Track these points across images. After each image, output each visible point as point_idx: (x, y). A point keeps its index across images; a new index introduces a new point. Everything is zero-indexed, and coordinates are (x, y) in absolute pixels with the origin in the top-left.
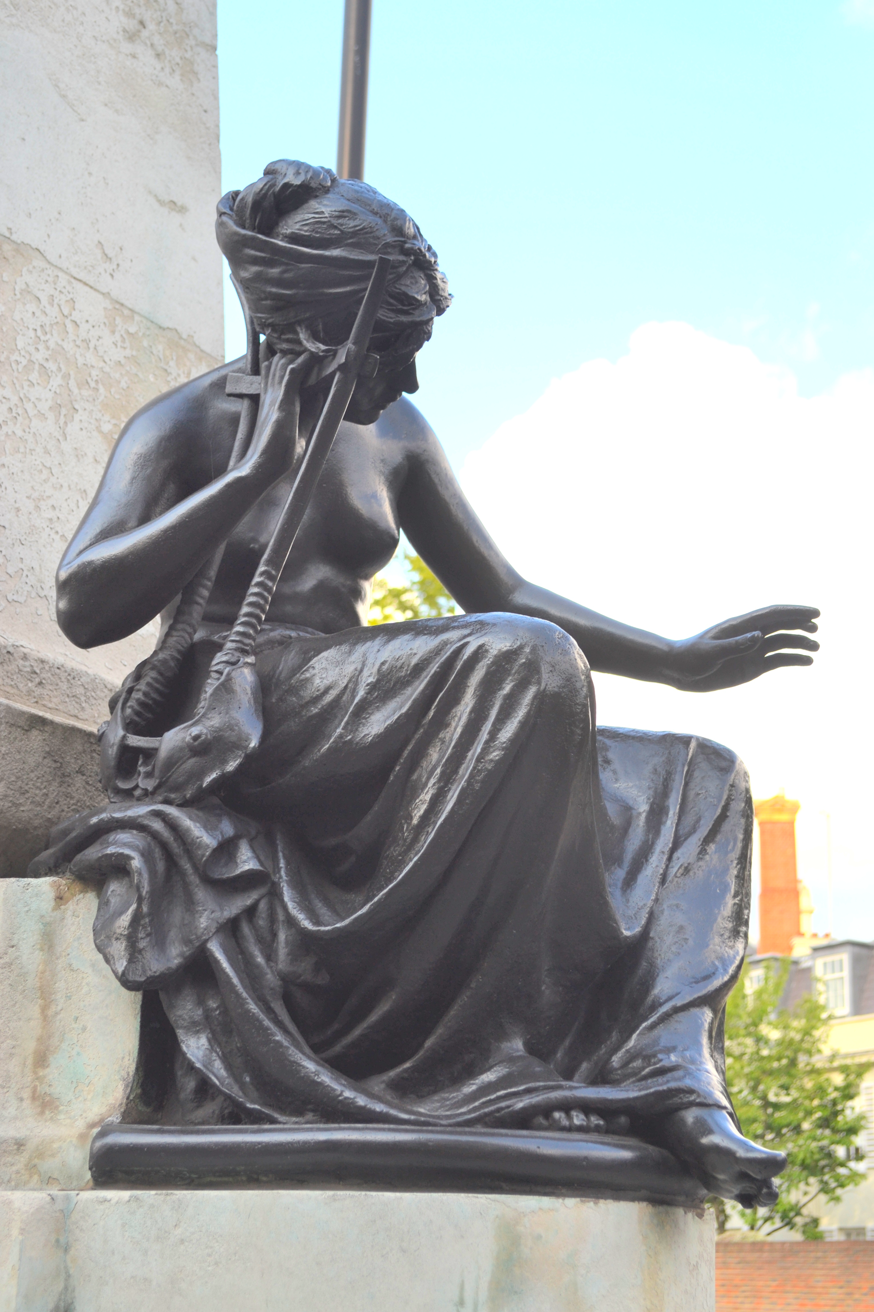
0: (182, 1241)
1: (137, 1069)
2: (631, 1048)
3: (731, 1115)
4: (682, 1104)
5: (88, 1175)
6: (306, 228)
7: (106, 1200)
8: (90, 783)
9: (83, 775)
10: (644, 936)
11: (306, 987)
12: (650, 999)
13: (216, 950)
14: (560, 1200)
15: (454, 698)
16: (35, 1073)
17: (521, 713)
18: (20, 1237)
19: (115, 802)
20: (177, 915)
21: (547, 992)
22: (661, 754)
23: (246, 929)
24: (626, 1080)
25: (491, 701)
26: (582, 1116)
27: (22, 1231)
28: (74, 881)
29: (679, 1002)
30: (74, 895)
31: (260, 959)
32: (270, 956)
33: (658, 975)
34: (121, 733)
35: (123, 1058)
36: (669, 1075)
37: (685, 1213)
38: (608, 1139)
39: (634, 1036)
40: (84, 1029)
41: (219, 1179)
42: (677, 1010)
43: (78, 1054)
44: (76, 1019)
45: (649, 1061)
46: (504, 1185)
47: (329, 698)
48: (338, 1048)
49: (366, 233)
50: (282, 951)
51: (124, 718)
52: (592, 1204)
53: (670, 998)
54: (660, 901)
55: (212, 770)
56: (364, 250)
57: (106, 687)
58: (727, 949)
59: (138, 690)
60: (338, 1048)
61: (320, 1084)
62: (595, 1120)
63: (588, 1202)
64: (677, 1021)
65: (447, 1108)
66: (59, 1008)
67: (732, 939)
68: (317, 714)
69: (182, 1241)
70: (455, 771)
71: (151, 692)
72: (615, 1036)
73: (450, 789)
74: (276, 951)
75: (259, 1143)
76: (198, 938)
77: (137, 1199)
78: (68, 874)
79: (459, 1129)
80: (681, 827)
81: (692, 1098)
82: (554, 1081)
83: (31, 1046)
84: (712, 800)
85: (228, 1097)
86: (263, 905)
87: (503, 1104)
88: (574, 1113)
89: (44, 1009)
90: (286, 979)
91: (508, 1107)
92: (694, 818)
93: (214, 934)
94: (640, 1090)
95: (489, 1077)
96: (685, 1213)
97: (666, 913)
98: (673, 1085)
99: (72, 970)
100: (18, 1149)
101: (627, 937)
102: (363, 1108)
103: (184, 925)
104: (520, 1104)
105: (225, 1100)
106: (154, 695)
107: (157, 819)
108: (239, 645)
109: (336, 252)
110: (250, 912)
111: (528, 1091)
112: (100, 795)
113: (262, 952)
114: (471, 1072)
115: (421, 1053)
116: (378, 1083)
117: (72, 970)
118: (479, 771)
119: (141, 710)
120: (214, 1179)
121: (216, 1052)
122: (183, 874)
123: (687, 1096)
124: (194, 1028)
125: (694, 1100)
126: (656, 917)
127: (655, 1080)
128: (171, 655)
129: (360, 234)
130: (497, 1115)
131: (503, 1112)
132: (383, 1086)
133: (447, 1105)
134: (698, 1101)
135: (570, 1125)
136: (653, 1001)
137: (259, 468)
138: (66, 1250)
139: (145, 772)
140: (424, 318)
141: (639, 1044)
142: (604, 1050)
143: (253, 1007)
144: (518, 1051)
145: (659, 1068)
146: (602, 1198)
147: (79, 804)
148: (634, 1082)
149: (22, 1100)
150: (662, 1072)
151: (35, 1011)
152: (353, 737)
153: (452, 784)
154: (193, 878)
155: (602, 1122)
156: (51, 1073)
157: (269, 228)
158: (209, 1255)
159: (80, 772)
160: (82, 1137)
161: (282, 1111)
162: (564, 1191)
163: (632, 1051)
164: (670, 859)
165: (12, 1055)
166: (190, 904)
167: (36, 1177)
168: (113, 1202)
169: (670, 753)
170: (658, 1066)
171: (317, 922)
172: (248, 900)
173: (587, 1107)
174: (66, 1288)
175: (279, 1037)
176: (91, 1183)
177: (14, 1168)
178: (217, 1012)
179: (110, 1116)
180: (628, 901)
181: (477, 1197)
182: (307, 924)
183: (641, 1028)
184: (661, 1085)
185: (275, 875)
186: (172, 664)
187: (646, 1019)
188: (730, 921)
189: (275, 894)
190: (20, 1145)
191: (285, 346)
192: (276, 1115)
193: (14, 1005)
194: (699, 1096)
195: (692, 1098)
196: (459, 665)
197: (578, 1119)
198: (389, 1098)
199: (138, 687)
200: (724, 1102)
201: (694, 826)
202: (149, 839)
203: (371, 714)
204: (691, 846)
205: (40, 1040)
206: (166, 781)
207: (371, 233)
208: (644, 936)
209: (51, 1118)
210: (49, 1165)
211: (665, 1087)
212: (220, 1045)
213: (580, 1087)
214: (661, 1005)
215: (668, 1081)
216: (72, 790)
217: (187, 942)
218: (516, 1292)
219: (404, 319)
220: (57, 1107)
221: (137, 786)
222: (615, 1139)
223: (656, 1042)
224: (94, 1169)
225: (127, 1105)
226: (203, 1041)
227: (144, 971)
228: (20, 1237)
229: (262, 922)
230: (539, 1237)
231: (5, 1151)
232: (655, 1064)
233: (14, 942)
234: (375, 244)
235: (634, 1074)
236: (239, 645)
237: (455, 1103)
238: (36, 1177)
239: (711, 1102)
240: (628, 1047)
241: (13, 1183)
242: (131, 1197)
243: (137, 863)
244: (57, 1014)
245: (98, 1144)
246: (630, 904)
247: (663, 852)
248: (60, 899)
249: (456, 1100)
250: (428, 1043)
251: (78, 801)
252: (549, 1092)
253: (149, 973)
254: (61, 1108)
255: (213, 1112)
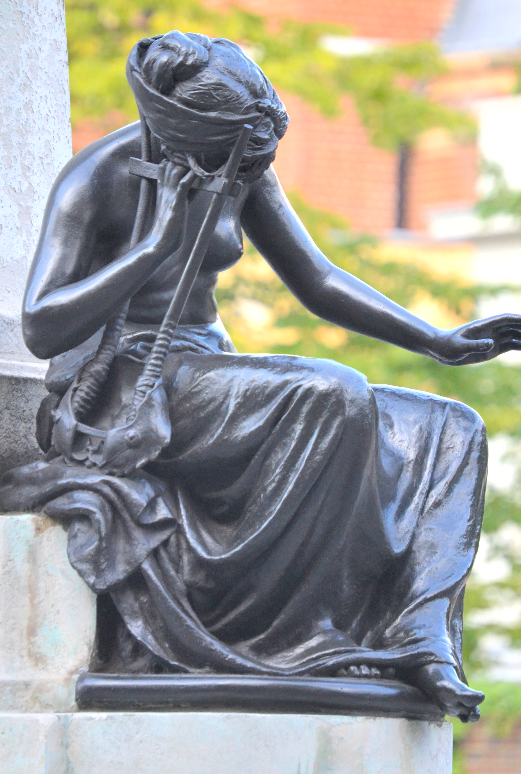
0: (141, 742)
1: (96, 638)
2: (397, 625)
3: (455, 668)
4: (426, 661)
5: (74, 703)
6: (194, 96)
7: (91, 719)
8: (13, 414)
9: (9, 409)
10: (409, 551)
11: (201, 590)
12: (410, 595)
13: (147, 567)
14: (354, 718)
15: (293, 419)
16: (29, 640)
17: (332, 432)
18: (45, 741)
19: (71, 467)
20: (121, 545)
21: (347, 589)
22: (425, 418)
23: (163, 554)
24: (393, 646)
25: (316, 424)
26: (367, 669)
27: (46, 737)
28: (47, 518)
29: (428, 595)
30: (47, 527)
31: (173, 573)
32: (178, 569)
33: (416, 577)
34: (74, 422)
35: (86, 631)
36: (420, 644)
37: (429, 724)
38: (382, 682)
39: (400, 617)
40: (58, 612)
41: (156, 706)
42: (427, 600)
43: (55, 628)
44: (53, 606)
45: (408, 634)
46: (322, 709)
47: (211, 407)
48: (218, 626)
49: (235, 101)
50: (186, 568)
51: (74, 409)
52: (372, 720)
53: (423, 593)
54: (420, 526)
55: (141, 457)
56: (233, 113)
57: (5, 322)
58: (462, 557)
59: (81, 390)
60: (218, 626)
61: (215, 650)
62: (375, 671)
63: (370, 718)
64: (426, 607)
65: (287, 662)
66: (41, 599)
67: (466, 550)
68: (203, 417)
69: (141, 742)
70: (294, 464)
71: (90, 392)
72: (388, 615)
73: (290, 476)
74: (182, 568)
75: (182, 686)
76: (136, 561)
77: (111, 718)
78: (42, 513)
79: (298, 678)
80: (435, 473)
81: (432, 658)
82: (351, 646)
83: (25, 623)
84: (457, 453)
85: (154, 656)
86: (173, 539)
87: (321, 662)
88: (362, 667)
89: (32, 599)
90: (189, 586)
91: (324, 664)
92: (445, 466)
93: (146, 558)
94: (401, 653)
95: (313, 642)
96: (429, 724)
97: (423, 534)
98: (421, 650)
99: (49, 575)
100: (26, 688)
101: (397, 554)
102: (240, 665)
103: (126, 553)
104: (331, 661)
105: (153, 657)
106: (92, 394)
107: (106, 486)
108: (154, 373)
109: (212, 114)
110: (165, 543)
111: (334, 653)
112: (19, 422)
113: (173, 567)
114: (300, 640)
115: (270, 630)
116: (244, 647)
117: (49, 575)
118: (308, 468)
119: (84, 404)
120: (153, 706)
121: (148, 630)
122: (124, 522)
123: (429, 657)
124: (134, 615)
125: (434, 659)
126: (416, 537)
127: (410, 647)
128: (103, 368)
129: (230, 102)
130: (317, 668)
131: (321, 667)
132: (247, 649)
133: (286, 661)
134: (436, 660)
135: (360, 674)
136: (413, 595)
137: (160, 247)
138: (67, 747)
139: (92, 451)
140: (271, 150)
141: (402, 622)
142: (381, 624)
143: (173, 604)
144: (328, 626)
145: (414, 639)
146: (378, 716)
147: (7, 432)
148: (398, 648)
149: (22, 657)
150: (416, 641)
151: (26, 601)
152: (228, 437)
153: (291, 472)
154: (131, 524)
155: (378, 672)
156: (39, 639)
157: (168, 91)
158: (158, 749)
159: (7, 408)
160: (67, 681)
161: (190, 665)
162: (356, 712)
163: (398, 627)
164: (427, 496)
165: (13, 629)
166: (129, 539)
167: (38, 705)
168: (97, 719)
169: (431, 417)
170: (413, 638)
171: (209, 553)
172: (162, 536)
173: (370, 663)
174: (68, 769)
175: (189, 622)
176: (75, 708)
177: (24, 699)
178: (147, 605)
179: (82, 667)
180: (398, 528)
181: (307, 717)
182: (204, 554)
183: (404, 612)
184: (413, 650)
185: (179, 519)
186: (104, 373)
187: (407, 606)
188: (465, 538)
189: (180, 531)
190: (27, 685)
191: (176, 160)
192: (188, 668)
193: (13, 597)
194: (436, 657)
195: (432, 658)
196: (296, 398)
197: (365, 670)
198: (251, 656)
199: (81, 388)
200: (452, 660)
201: (445, 472)
202: (101, 498)
203: (240, 423)
204: (440, 488)
205: (30, 619)
206: (111, 461)
207: (237, 100)
208: (409, 551)
209: (43, 668)
210: (46, 697)
211: (416, 652)
212: (149, 625)
213: (366, 651)
214: (417, 597)
215: (418, 648)
216: (3, 422)
217: (128, 563)
218: (329, 769)
219: (259, 153)
220: (45, 661)
221: (87, 459)
222: (386, 682)
223: (414, 621)
224: (79, 700)
225: (91, 660)
226: (140, 623)
227: (105, 583)
228: (45, 741)
229: (173, 549)
230: (342, 739)
231: (18, 689)
232: (411, 636)
233: (11, 558)
234: (241, 108)
235: (397, 642)
236: (154, 373)
237: (291, 659)
238: (38, 705)
239: (443, 660)
240: (396, 624)
241: (24, 708)
242: (108, 717)
243: (99, 516)
244: (40, 602)
245: (81, 685)
246: (399, 530)
247: (422, 494)
248: (38, 530)
249: (292, 657)
250: (275, 623)
251: (6, 430)
252: (348, 655)
253: (108, 584)
254: (48, 662)
255: (145, 665)
